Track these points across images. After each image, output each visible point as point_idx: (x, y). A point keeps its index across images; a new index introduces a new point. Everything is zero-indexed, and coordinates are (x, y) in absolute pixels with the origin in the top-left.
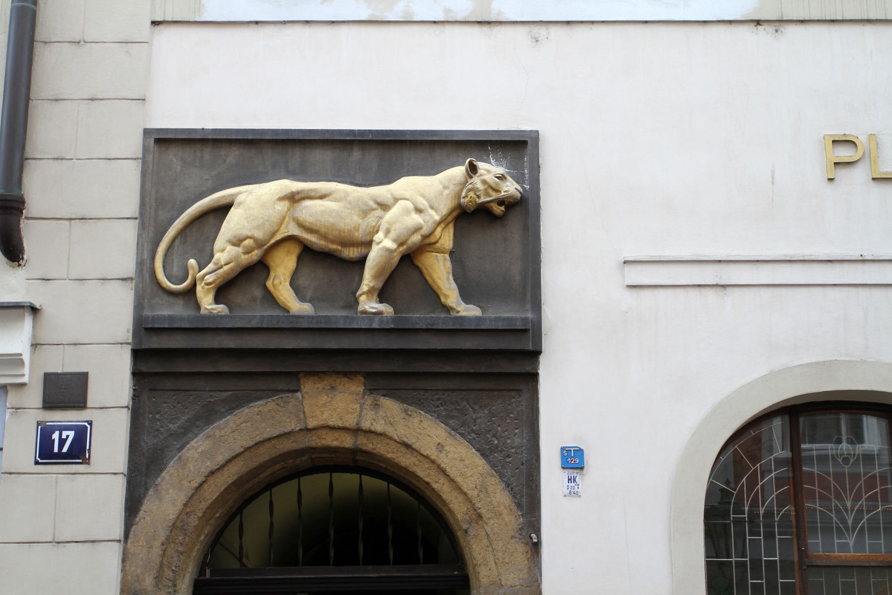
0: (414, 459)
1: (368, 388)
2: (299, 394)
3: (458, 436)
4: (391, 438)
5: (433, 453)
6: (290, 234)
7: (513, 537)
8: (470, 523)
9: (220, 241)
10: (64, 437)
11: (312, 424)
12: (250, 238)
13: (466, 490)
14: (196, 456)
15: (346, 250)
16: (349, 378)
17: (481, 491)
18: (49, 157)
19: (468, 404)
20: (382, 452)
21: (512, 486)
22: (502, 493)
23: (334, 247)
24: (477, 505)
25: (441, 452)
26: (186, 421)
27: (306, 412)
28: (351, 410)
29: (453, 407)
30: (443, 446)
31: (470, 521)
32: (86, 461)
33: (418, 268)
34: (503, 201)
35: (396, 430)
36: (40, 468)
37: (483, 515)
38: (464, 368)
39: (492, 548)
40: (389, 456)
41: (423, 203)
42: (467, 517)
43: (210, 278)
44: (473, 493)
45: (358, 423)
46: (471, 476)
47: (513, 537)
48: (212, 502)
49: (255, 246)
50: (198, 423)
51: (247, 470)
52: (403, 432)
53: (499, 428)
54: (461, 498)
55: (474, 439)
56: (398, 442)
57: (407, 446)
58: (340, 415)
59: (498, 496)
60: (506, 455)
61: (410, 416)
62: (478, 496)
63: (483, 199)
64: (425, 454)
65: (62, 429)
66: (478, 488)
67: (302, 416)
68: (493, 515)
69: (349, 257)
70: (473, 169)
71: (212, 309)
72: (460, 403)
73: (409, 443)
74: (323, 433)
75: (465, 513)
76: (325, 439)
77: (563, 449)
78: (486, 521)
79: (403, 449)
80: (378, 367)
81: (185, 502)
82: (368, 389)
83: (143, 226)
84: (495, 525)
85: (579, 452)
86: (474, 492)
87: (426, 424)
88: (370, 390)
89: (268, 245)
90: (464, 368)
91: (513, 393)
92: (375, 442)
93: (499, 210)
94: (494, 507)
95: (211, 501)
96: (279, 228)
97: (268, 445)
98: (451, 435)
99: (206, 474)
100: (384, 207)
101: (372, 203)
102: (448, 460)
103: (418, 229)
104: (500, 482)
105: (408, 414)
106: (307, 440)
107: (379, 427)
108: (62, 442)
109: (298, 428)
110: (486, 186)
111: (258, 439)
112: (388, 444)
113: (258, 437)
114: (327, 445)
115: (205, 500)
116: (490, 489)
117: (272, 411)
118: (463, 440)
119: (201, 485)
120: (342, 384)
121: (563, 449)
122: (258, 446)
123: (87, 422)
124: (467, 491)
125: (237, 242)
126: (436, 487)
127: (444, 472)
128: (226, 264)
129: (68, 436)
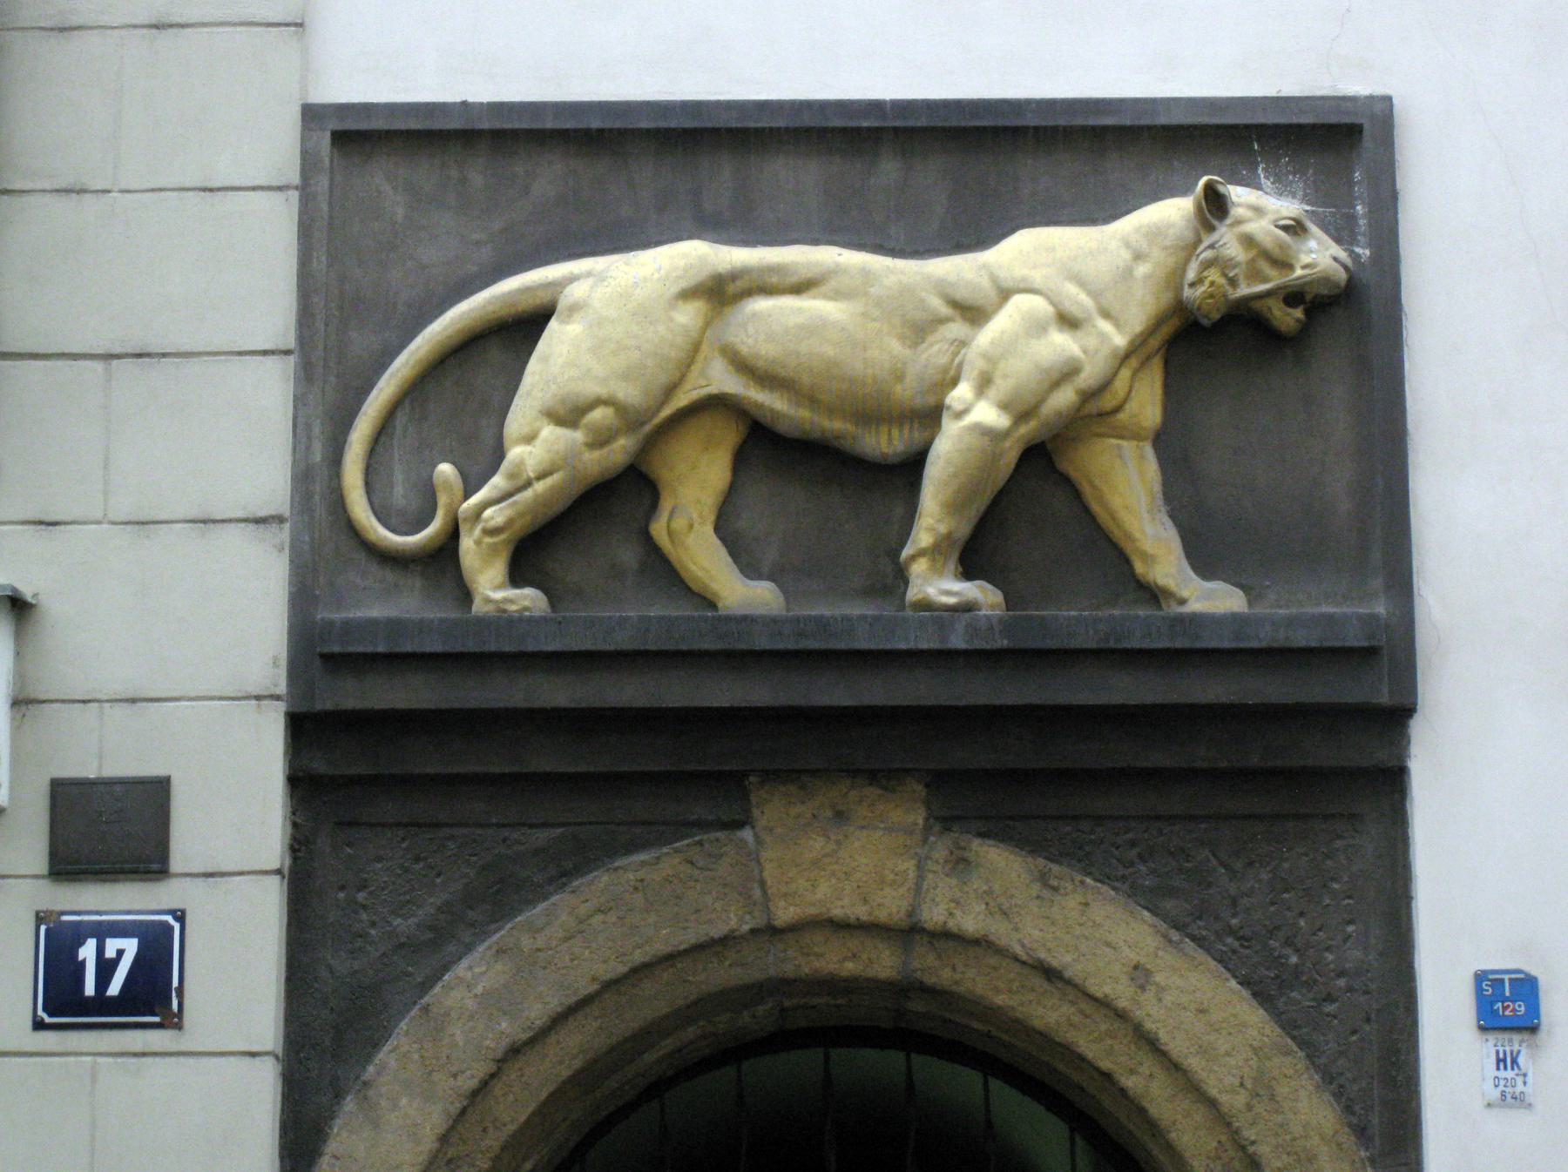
0: (1067, 1009)
2: (747, 834)
4: (1001, 952)
5: (1121, 992)
9: (523, 412)
10: (110, 953)
11: (785, 914)
13: (1213, 1092)
17: (1257, 1095)
21: (1342, 1080)
28: (891, 876)
32: (173, 1021)
35: (1016, 929)
36: (50, 1040)
37: (1264, 1161)
38: (1202, 755)
40: (1000, 1000)
41: (1077, 298)
44: (1233, 1101)
46: (1228, 1054)
51: (608, 1041)
53: (1302, 923)
54: (1200, 1114)
56: (1024, 963)
57: (1050, 974)
62: (1249, 1108)
63: (1244, 290)
64: (1099, 995)
65: (103, 932)
66: (1249, 1086)
70: (1215, 206)
73: (1055, 963)
76: (822, 955)
77: (1480, 977)
79: (1038, 981)
83: (307, 374)
85: (1526, 987)
87: (1099, 911)
93: (1287, 318)
95: (512, 1128)
98: (1170, 941)
100: (974, 313)
101: (938, 305)
102: (1162, 1012)
103: (1067, 372)
108: (106, 968)
109: (746, 928)
110: (1254, 252)
111: (638, 957)
112: (995, 969)
114: (826, 971)
116: (1283, 1090)
118: (1202, 956)
119: (485, 1085)
121: (1480, 977)
123: (172, 912)
124: (1218, 1096)
125: (568, 414)
127: (1150, 1043)
128: (542, 476)
129: (120, 953)
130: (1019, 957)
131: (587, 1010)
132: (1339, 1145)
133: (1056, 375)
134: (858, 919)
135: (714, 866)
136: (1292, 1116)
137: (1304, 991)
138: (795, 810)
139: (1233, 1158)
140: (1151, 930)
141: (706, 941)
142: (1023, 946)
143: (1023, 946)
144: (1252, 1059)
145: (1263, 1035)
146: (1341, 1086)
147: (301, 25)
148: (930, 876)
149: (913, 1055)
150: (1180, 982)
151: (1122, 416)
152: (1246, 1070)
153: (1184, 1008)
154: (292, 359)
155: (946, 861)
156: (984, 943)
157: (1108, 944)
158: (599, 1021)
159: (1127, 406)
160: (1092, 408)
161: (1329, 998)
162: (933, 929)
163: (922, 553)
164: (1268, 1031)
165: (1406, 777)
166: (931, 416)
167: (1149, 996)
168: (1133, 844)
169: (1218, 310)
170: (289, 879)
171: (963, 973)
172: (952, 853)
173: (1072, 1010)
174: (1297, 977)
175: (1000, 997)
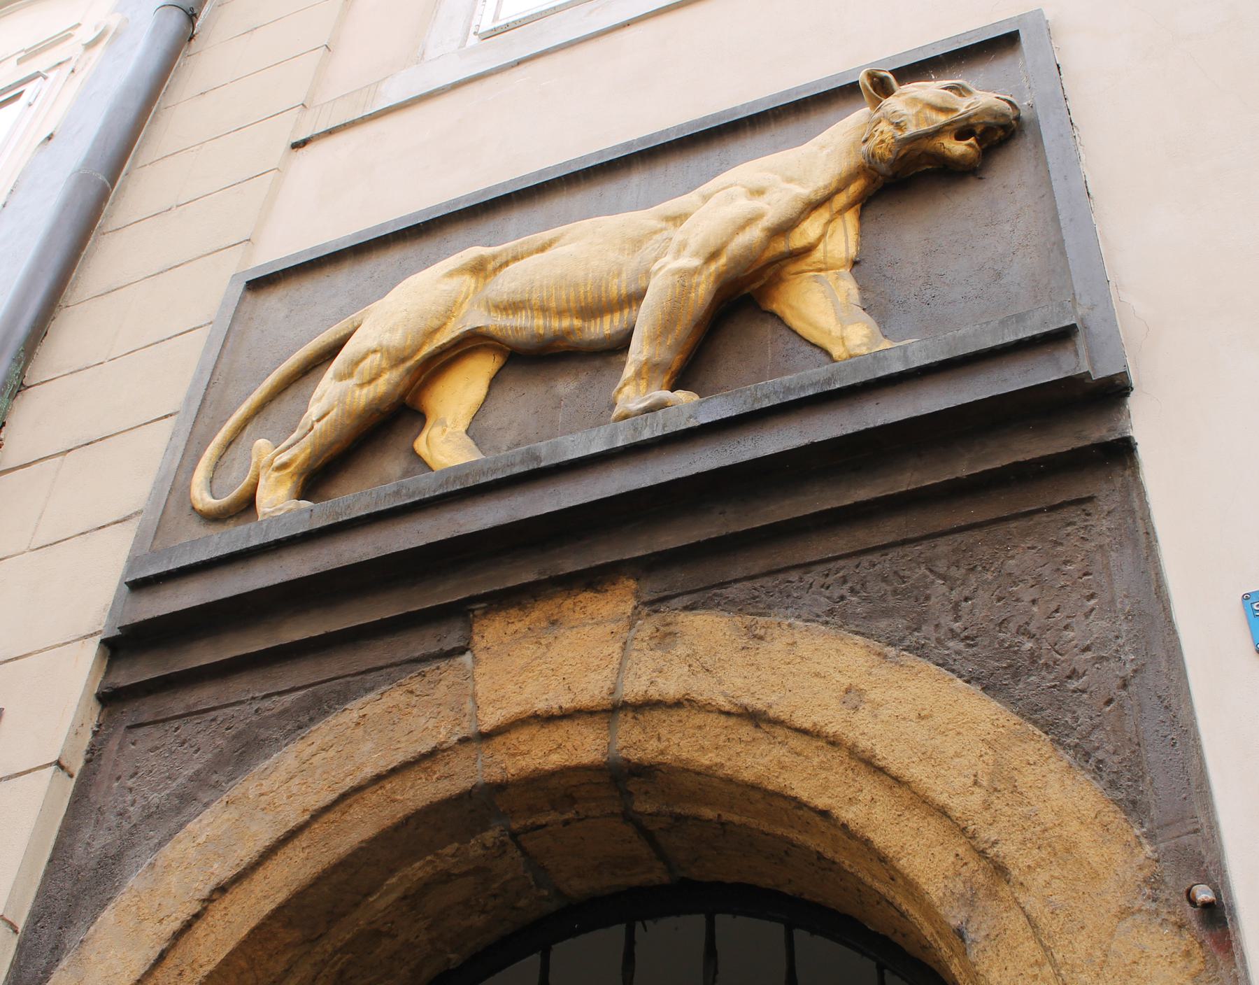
0: (778, 752)
1: (647, 598)
2: (467, 658)
3: (908, 658)
4: (705, 708)
5: (832, 719)
6: (467, 329)
7: (1125, 913)
8: (971, 903)
11: (490, 719)
12: (375, 351)
13: (942, 799)
14: (192, 853)
15: (596, 324)
16: (598, 591)
17: (995, 790)
18: (66, 372)
19: (931, 571)
20: (684, 755)
21: (1100, 755)
22: (1069, 782)
23: (566, 323)
24: (984, 835)
25: (856, 708)
26: (191, 779)
27: (480, 695)
28: (596, 662)
29: (889, 588)
30: (861, 692)
31: (969, 895)
33: (780, 320)
34: (968, 125)
35: (720, 682)
37: (1009, 863)
38: (907, 480)
39: (1054, 964)
40: (706, 760)
42: (960, 886)
44: (965, 803)
45: (615, 689)
46: (957, 755)
47: (1125, 913)
48: (211, 972)
49: (384, 364)
50: (215, 777)
51: (315, 870)
52: (739, 682)
53: (1035, 609)
54: (932, 829)
55: (958, 653)
56: (728, 714)
57: (754, 717)
58: (567, 681)
59: (1054, 791)
60: (1068, 673)
61: (761, 638)
62: (987, 806)
64: (807, 725)
66: (985, 783)
67: (469, 706)
68: (1044, 854)
69: (601, 336)
72: (907, 573)
73: (760, 706)
74: (522, 738)
75: (949, 874)
76: (529, 752)
78: (1021, 879)
79: (746, 731)
80: (669, 539)
81: (138, 978)
82: (645, 604)
84: (1056, 884)
86: (972, 798)
87: (806, 646)
88: (652, 603)
89: (419, 357)
90: (907, 480)
91: (1065, 514)
92: (663, 731)
94: (1045, 830)
95: (210, 967)
96: (445, 324)
97: (372, 797)
98: (885, 657)
99: (205, 893)
102: (878, 727)
104: (1055, 750)
105: (755, 636)
106: (479, 765)
107: (672, 687)
109: (455, 738)
110: (920, 106)
111: (349, 783)
112: (700, 727)
113: (348, 779)
114: (533, 767)
115: (196, 966)
116: (1026, 779)
117: (394, 710)
118: (922, 664)
120: (577, 609)
122: (348, 801)
124: (948, 801)
126: (850, 816)
127: (870, 765)
130: (723, 709)
131: (296, 842)
132: (1105, 827)
133: (741, 221)
134: (561, 708)
135: (432, 691)
136: (1041, 805)
137: (1044, 673)
138: (512, 628)
139: (974, 872)
140: (864, 650)
141: (413, 757)
142: (726, 696)
143: (726, 696)
144: (986, 754)
145: (998, 726)
146: (1101, 761)
147: (249, 240)
148: (635, 654)
149: (720, 919)
150: (897, 694)
151: (818, 255)
152: (981, 765)
153: (904, 719)
155: (651, 639)
156: (685, 702)
157: (817, 675)
158: (307, 851)
159: (821, 246)
160: (781, 246)
161: (1073, 675)
162: (633, 700)
164: (1002, 721)
165: (1135, 454)
167: (864, 713)
168: (844, 580)
169: (890, 151)
170: (77, 779)
171: (668, 740)
172: (658, 630)
173: (784, 751)
174: (1034, 662)
175: (707, 757)
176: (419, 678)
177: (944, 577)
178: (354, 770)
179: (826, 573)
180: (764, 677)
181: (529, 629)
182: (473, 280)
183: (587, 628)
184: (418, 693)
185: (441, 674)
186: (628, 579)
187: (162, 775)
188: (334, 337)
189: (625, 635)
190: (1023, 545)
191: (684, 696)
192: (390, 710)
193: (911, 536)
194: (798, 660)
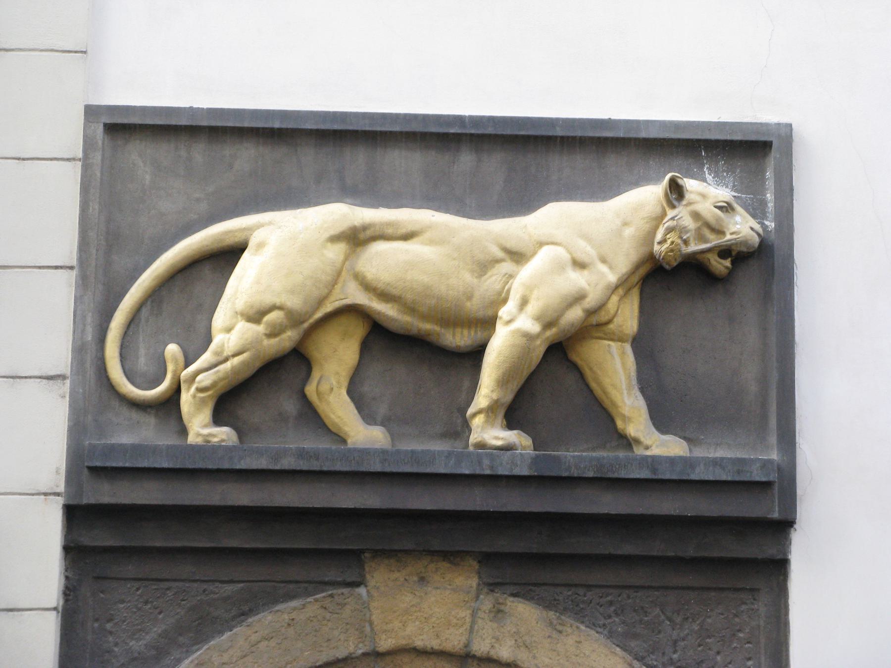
2: (362, 590)
11: (385, 644)
23: (427, 326)
28: (455, 621)
38: (657, 548)
41: (585, 251)
43: (205, 379)
52: (547, 661)
63: (694, 247)
67: (368, 629)
70: (676, 191)
71: (210, 435)
80: (504, 544)
89: (311, 321)
93: (721, 266)
100: (518, 257)
103: (579, 297)
141: (333, 660)
154: (74, 273)
159: (615, 320)
160: (594, 320)
163: (480, 412)
166: (489, 323)
168: (611, 603)
176: (330, 599)
177: (670, 620)
178: (292, 661)
179: (601, 595)
180: (561, 661)
181: (406, 580)
182: (545, 612)
183: (448, 592)
184: (331, 610)
185: (345, 599)
186: (474, 559)
187: (136, 627)
188: (216, 245)
189: (473, 604)
190: (658, 443)
191: (513, 661)
192: (311, 619)
193: (653, 584)
194: (582, 655)
